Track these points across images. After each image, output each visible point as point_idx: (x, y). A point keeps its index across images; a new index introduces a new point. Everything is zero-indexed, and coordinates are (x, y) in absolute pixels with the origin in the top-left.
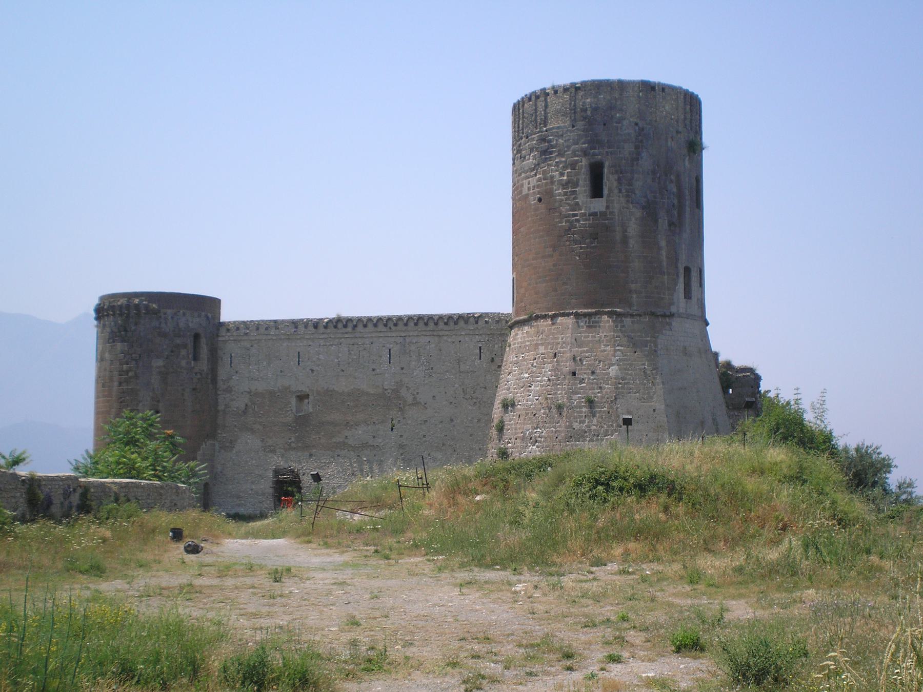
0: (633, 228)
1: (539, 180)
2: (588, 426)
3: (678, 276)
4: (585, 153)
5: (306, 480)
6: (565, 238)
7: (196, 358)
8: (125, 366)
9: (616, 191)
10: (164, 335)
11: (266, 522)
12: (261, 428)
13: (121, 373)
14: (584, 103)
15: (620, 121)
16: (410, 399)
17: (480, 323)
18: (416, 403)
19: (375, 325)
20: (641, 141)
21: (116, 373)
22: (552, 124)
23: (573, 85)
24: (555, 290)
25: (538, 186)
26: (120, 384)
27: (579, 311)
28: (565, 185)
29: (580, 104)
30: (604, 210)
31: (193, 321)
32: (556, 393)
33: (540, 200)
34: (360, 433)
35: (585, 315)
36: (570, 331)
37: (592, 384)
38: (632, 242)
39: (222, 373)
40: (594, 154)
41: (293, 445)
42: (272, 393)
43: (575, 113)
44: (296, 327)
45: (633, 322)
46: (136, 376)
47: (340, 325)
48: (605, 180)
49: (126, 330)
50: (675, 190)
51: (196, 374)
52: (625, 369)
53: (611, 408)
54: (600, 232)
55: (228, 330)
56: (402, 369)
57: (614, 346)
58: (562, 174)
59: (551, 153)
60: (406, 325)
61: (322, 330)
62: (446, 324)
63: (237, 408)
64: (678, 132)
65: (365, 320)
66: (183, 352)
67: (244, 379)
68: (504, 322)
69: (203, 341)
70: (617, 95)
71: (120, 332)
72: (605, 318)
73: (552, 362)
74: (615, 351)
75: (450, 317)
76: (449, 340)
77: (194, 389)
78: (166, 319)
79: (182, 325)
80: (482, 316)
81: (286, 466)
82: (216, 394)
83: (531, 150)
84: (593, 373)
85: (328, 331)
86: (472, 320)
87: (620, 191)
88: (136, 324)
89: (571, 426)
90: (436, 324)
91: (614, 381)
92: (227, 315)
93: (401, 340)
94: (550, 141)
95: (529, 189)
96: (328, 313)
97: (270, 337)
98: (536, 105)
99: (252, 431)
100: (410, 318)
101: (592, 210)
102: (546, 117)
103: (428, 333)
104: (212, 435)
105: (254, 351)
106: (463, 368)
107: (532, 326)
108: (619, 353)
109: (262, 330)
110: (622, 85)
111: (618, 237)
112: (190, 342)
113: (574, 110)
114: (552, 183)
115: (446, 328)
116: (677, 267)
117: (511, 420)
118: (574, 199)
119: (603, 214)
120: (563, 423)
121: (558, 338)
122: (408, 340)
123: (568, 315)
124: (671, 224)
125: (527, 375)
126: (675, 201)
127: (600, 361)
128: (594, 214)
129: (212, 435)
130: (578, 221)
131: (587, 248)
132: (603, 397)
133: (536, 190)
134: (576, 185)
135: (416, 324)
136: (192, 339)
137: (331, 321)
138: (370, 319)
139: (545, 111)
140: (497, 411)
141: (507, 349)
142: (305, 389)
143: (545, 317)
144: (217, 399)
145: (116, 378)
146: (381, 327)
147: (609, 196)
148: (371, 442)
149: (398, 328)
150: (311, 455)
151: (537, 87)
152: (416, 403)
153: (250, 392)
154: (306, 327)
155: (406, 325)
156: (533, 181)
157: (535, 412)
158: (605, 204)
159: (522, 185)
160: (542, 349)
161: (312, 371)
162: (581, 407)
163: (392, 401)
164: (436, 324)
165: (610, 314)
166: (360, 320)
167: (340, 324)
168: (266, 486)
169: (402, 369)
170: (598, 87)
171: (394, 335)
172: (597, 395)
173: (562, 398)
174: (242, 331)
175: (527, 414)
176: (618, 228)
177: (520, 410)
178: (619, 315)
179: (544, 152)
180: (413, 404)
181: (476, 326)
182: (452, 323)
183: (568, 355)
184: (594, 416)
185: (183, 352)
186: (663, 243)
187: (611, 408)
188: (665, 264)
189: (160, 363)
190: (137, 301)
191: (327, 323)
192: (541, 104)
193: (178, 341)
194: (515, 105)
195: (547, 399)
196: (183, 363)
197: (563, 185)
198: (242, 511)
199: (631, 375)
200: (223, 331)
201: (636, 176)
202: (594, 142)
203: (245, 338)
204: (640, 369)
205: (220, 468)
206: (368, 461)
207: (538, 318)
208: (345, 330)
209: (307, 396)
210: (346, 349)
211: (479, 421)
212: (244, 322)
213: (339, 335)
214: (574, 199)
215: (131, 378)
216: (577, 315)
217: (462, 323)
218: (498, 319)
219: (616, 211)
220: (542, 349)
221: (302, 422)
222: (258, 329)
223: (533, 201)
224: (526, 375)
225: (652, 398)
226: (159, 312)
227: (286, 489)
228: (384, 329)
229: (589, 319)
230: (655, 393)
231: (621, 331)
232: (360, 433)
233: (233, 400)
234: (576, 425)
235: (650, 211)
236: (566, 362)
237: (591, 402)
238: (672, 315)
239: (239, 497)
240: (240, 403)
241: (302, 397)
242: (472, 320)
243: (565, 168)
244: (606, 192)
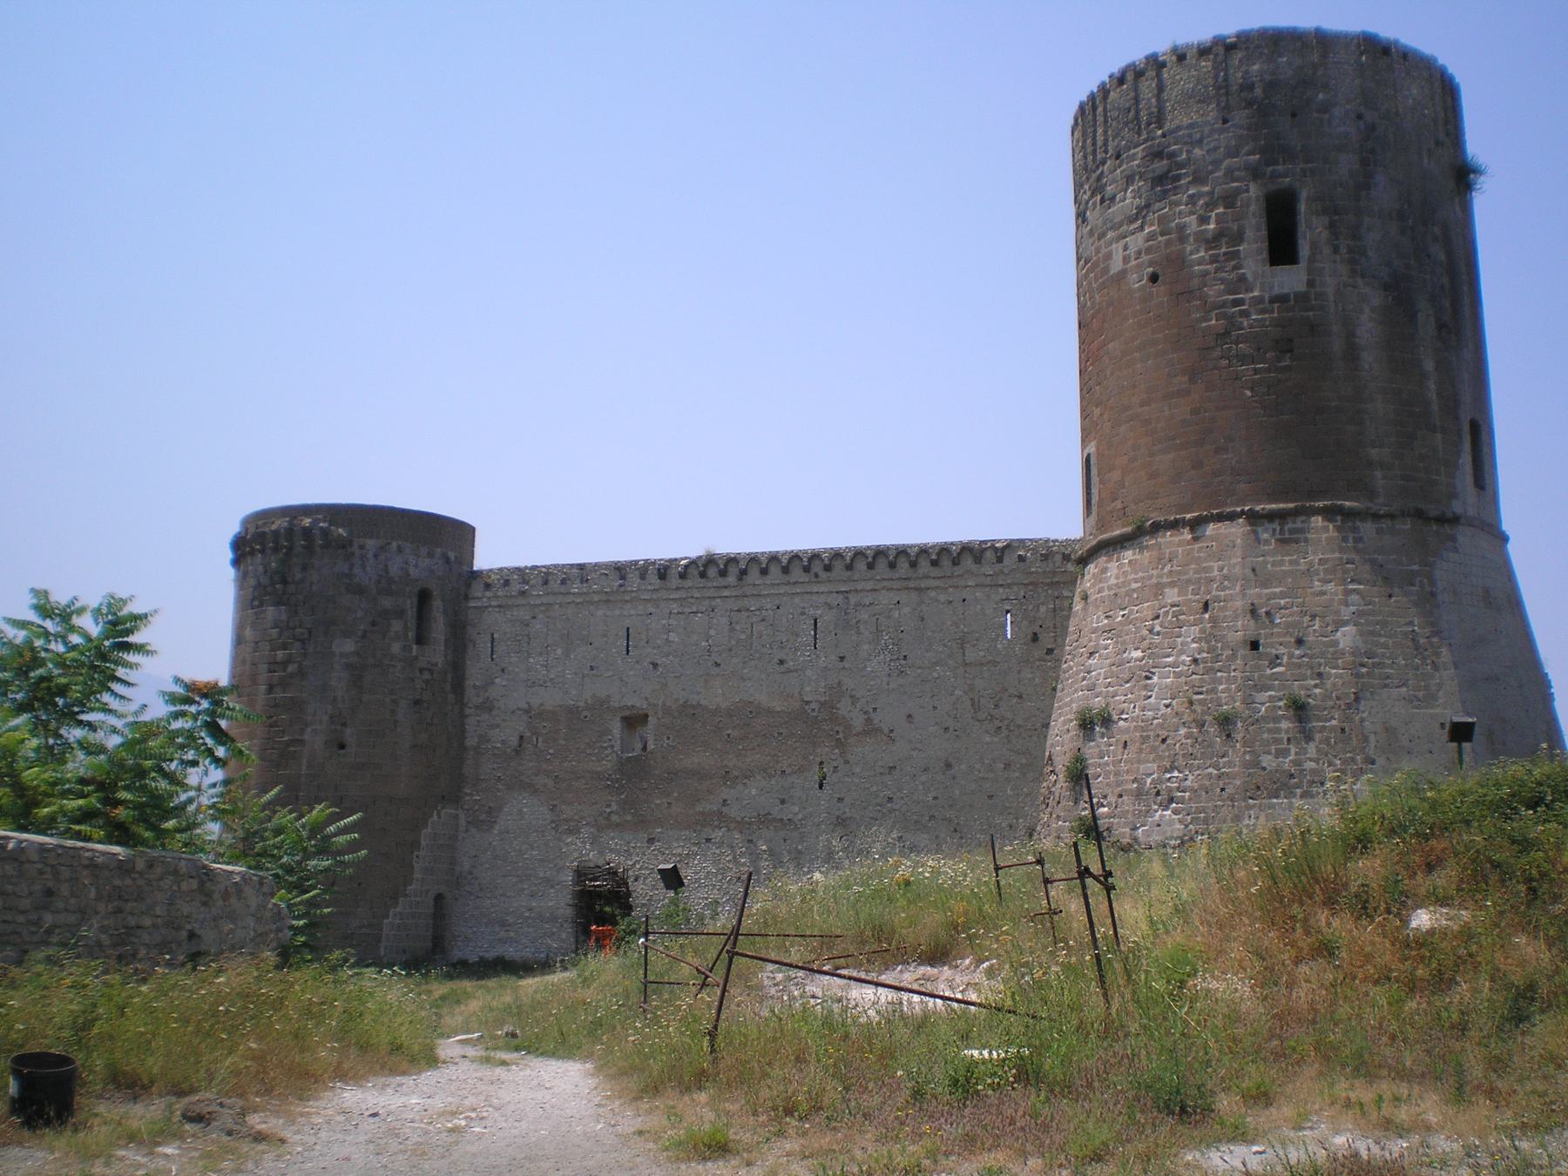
0: (1368, 329)
1: (1151, 237)
2: (1297, 763)
3: (1460, 437)
4: (1255, 173)
5: (647, 892)
6: (1217, 353)
7: (421, 640)
8: (280, 653)
9: (1327, 250)
10: (360, 591)
11: (557, 977)
12: (550, 783)
13: (273, 665)
14: (1247, 72)
15: (1325, 108)
16: (858, 722)
17: (1007, 561)
18: (871, 730)
19: (786, 570)
20: (1372, 151)
21: (263, 668)
22: (1177, 119)
23: (1218, 41)
24: (1198, 465)
25: (1148, 251)
26: (271, 688)
27: (1258, 508)
28: (1213, 241)
29: (1237, 77)
30: (1302, 288)
31: (419, 565)
32: (1214, 690)
33: (1154, 278)
34: (754, 795)
35: (1271, 516)
36: (1239, 552)
37: (1299, 666)
38: (1368, 358)
39: (475, 673)
40: (1274, 176)
41: (614, 818)
42: (572, 712)
43: (1227, 94)
44: (623, 578)
45: (1379, 531)
46: (302, 673)
47: (712, 572)
48: (1302, 227)
49: (284, 582)
50: (1442, 257)
51: (421, 671)
52: (1372, 633)
53: (1348, 719)
54: (1296, 336)
55: (488, 586)
56: (842, 659)
57: (1343, 582)
58: (1203, 220)
59: (1178, 178)
60: (849, 567)
61: (674, 581)
62: (935, 563)
63: (503, 742)
64: (1438, 143)
65: (764, 560)
66: (397, 626)
67: (519, 683)
68: (1058, 558)
69: (437, 604)
70: (1315, 58)
71: (273, 584)
72: (1318, 521)
73: (1201, 621)
74: (1347, 593)
75: (944, 549)
76: (942, 598)
77: (417, 702)
78: (363, 557)
79: (394, 571)
80: (1010, 546)
81: (601, 862)
82: (463, 716)
83: (1129, 179)
84: (1300, 642)
85: (688, 583)
86: (989, 555)
87: (1336, 250)
88: (304, 568)
89: (1256, 763)
90: (913, 565)
91: (1349, 658)
92: (486, 557)
93: (836, 600)
94: (1172, 155)
95: (1126, 260)
96: (685, 546)
97: (569, 599)
98: (1136, 89)
99: (535, 791)
100: (859, 553)
101: (1277, 291)
102: (1161, 109)
103: (896, 585)
104: (453, 797)
105: (537, 626)
106: (971, 655)
107: (1142, 549)
108: (1355, 597)
109: (554, 585)
110: (1322, 42)
111: (1337, 346)
112: (410, 605)
113: (1223, 88)
114: (1182, 239)
115: (935, 572)
116: (1457, 418)
117: (1102, 756)
118: (1235, 268)
119: (1302, 298)
120: (1237, 755)
121: (1210, 569)
122: (853, 599)
123: (1232, 517)
124: (1441, 326)
125: (1139, 654)
126: (1445, 280)
127: (1313, 617)
128: (1282, 299)
129: (453, 797)
130: (1245, 314)
131: (1269, 370)
132: (1326, 697)
133: (1145, 258)
134: (1238, 238)
135: (871, 566)
136: (415, 600)
137: (693, 562)
138: (774, 558)
139: (1158, 96)
140: (1061, 738)
141: (1078, 607)
142: (640, 704)
143: (1174, 525)
144: (463, 725)
145: (263, 677)
146: (797, 573)
147: (1312, 259)
148: (775, 812)
149: (833, 574)
150: (651, 841)
151: (1136, 53)
152: (871, 730)
153: (527, 711)
154: (643, 577)
155: (849, 567)
156: (1137, 242)
157: (1164, 733)
158: (1305, 278)
159: (1109, 256)
160: (1172, 595)
161: (655, 665)
162: (1277, 719)
163: (821, 726)
164: (913, 565)
165: (1329, 513)
166: (753, 559)
167: (711, 568)
168: (560, 901)
169: (842, 659)
170: (1274, 41)
171: (823, 588)
172: (1314, 693)
173: (1228, 696)
174: (516, 587)
175: (1145, 739)
176: (1335, 328)
177: (1127, 731)
178: (1349, 515)
179: (1160, 180)
180: (866, 733)
181: (999, 566)
182: (946, 562)
183: (1239, 603)
184: (1309, 738)
185: (397, 626)
186: (1429, 365)
187: (1348, 719)
188: (1435, 408)
189: (349, 646)
190: (307, 522)
191: (686, 566)
192: (1147, 87)
193: (387, 603)
194: (1082, 107)
195: (1191, 703)
196: (396, 648)
197: (1207, 242)
198: (510, 952)
199: (1385, 646)
200: (477, 589)
201: (1366, 220)
202: (1274, 151)
203: (521, 601)
204: (1405, 634)
205: (466, 864)
206: (771, 852)
207: (1156, 528)
208: (721, 581)
209: (643, 719)
210: (725, 620)
211: (1007, 766)
212: (518, 569)
213: (711, 593)
214: (1235, 268)
215: (291, 676)
216: (1254, 518)
217: (968, 562)
218: (1047, 552)
219: (1330, 291)
220: (1172, 595)
221: (633, 774)
222: (546, 583)
223: (1136, 282)
224: (1131, 655)
225: (1434, 697)
226: (351, 543)
227: (601, 909)
228: (804, 578)
229: (1282, 524)
230: (1440, 686)
231: (1357, 551)
232: (754, 795)
233: (493, 727)
234: (1267, 761)
235: (1399, 296)
236: (1235, 618)
237: (1299, 709)
238: (1455, 520)
239: (503, 924)
240: (508, 733)
241: (634, 721)
242: (989, 555)
243: (1210, 206)
244: (1304, 251)
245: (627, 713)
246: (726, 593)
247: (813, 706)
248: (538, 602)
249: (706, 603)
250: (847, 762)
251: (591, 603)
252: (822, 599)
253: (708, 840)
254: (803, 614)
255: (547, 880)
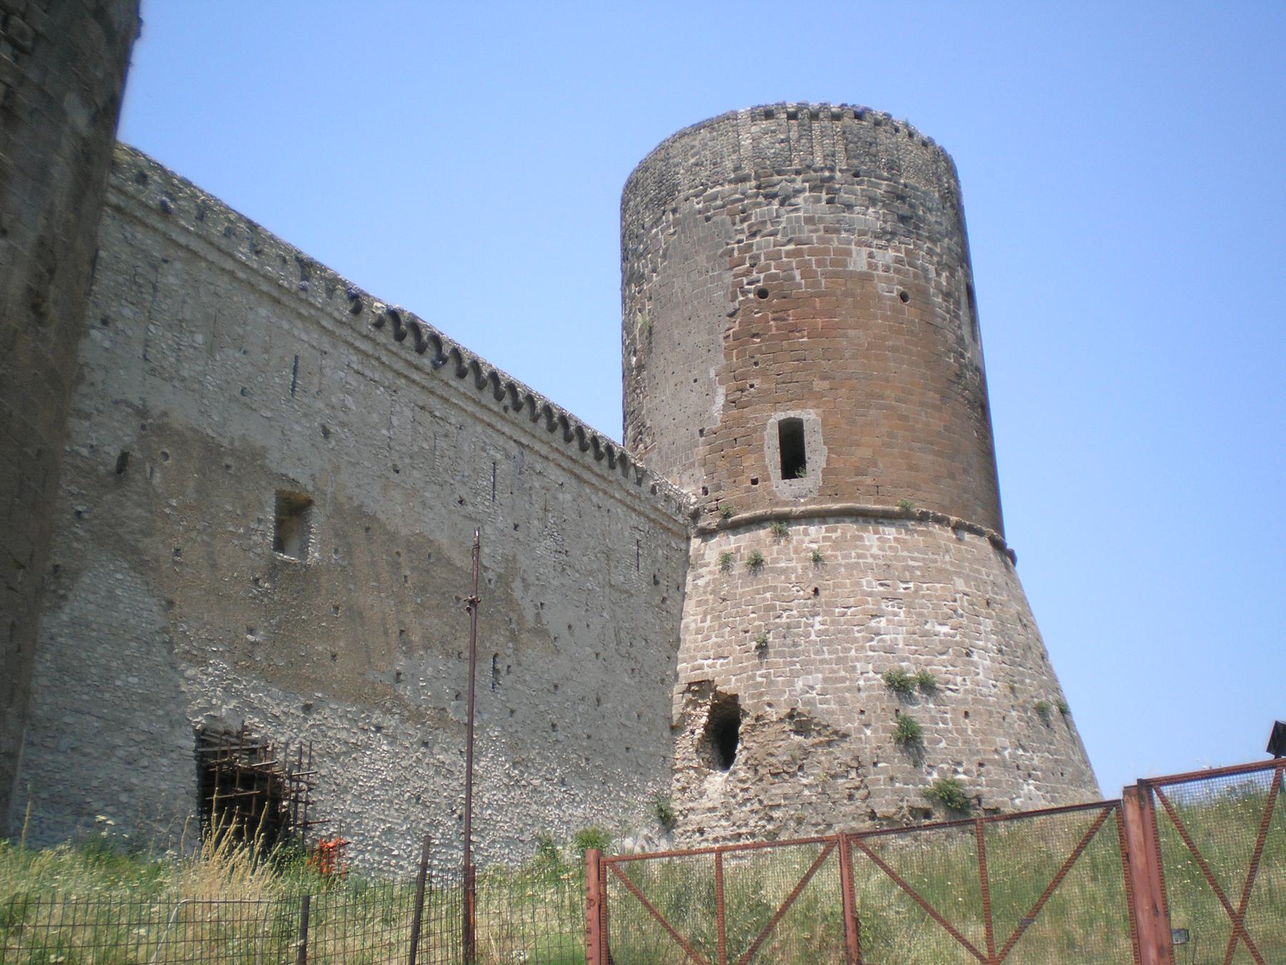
161: (326, 433)
174: (153, 196)
203: (154, 220)
213: (400, 366)
245: (288, 488)
246: (415, 376)
247: (490, 575)
248: (183, 240)
249: (390, 375)
250: (519, 664)
251: (253, 288)
252: (501, 441)
253: (379, 729)
254: (483, 450)
255: (153, 738)
